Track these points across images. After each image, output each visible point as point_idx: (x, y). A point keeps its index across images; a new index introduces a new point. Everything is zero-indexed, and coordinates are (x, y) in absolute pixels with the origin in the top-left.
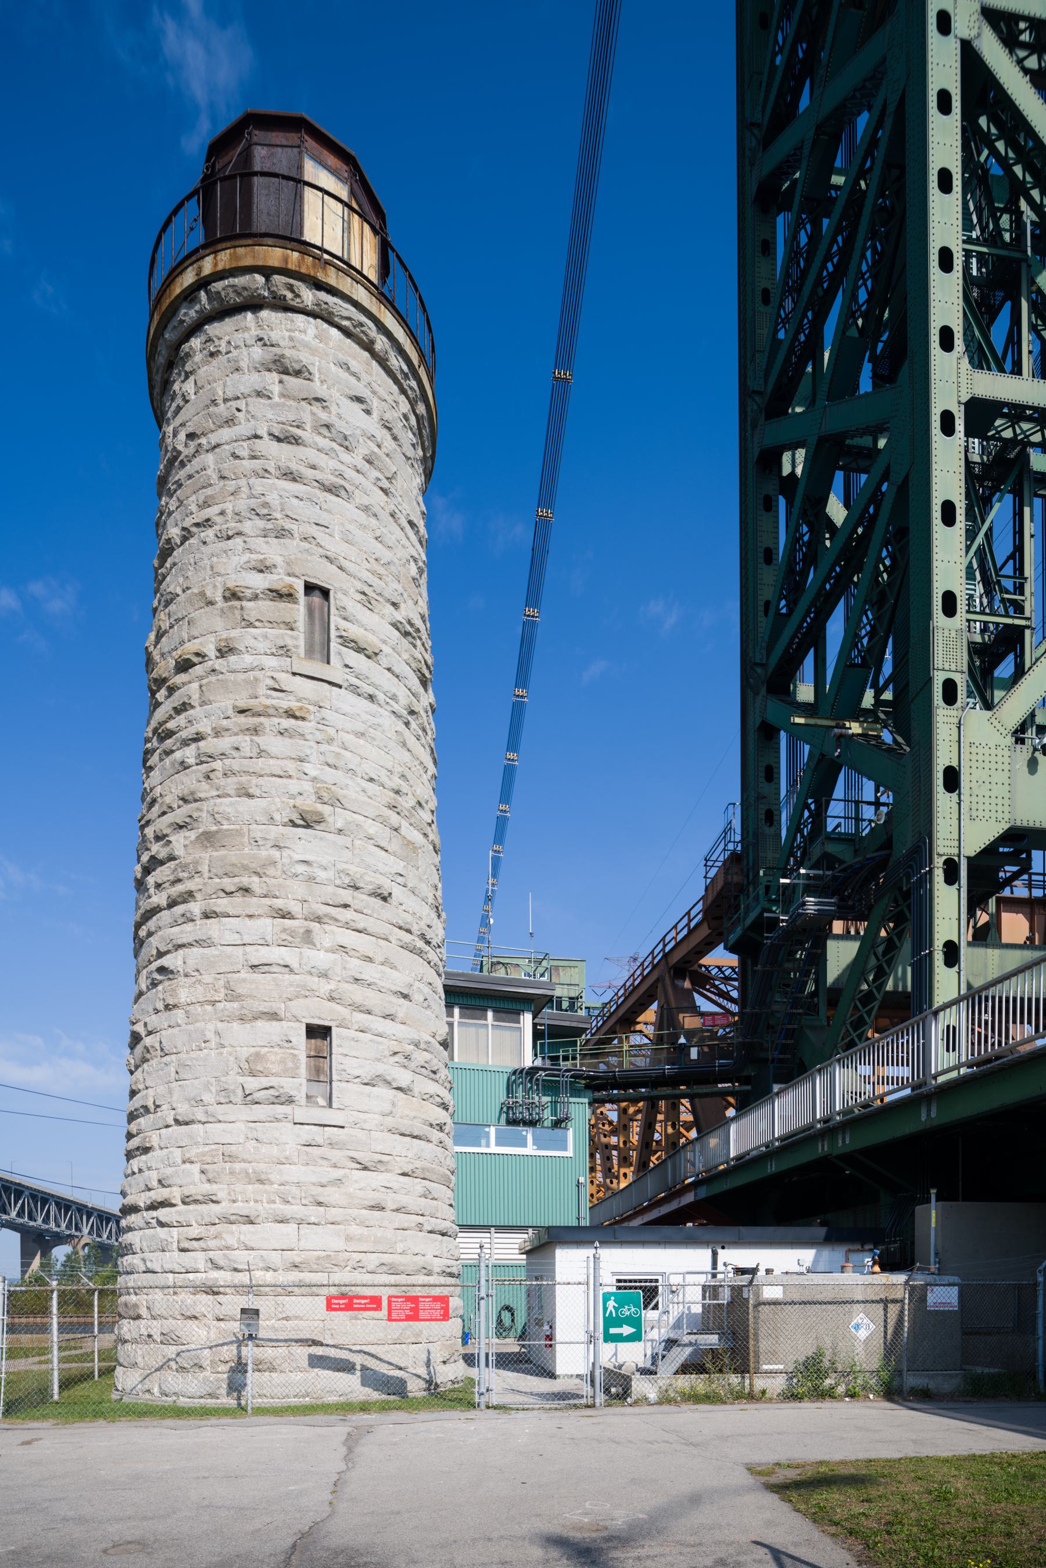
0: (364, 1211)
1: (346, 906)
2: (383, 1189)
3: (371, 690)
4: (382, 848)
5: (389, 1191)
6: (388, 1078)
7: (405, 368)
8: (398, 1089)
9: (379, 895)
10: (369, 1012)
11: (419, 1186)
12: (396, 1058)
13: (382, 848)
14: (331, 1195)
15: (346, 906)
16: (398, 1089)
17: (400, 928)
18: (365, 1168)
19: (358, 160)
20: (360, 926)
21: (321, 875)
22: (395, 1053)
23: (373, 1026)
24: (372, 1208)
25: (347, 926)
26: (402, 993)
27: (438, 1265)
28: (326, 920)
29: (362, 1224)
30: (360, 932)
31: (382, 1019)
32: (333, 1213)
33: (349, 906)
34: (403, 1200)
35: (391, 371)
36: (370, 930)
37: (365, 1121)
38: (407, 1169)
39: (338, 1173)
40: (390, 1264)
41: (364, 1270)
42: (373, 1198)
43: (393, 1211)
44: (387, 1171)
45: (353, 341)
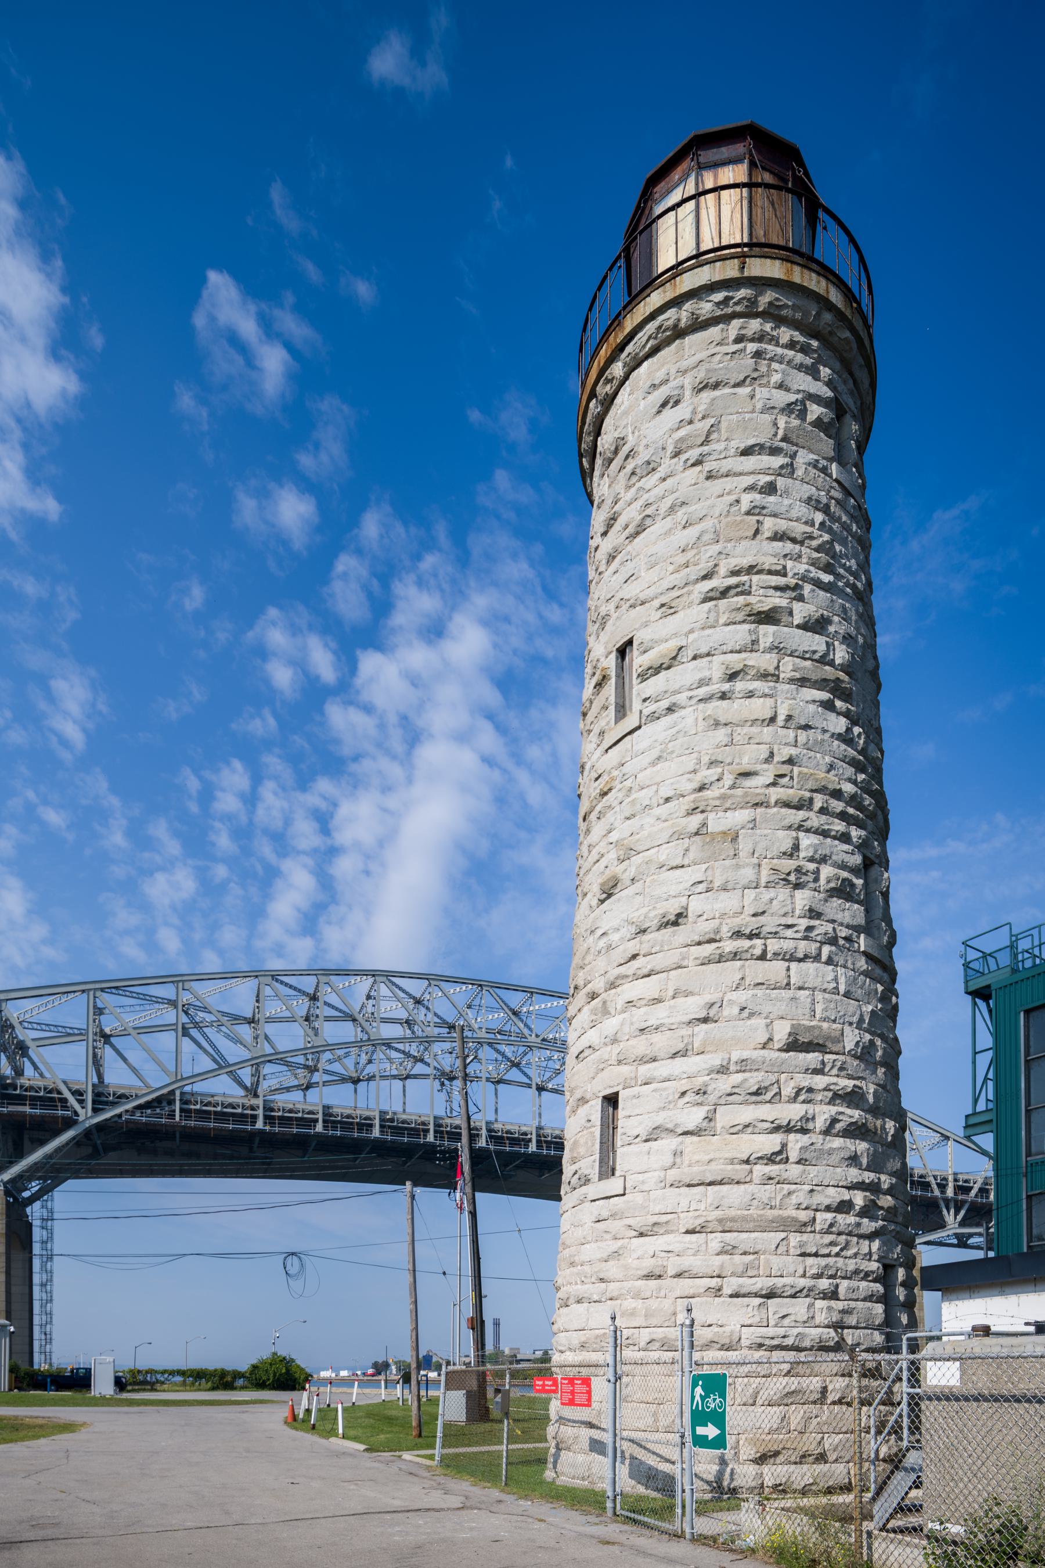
0: (640, 1282)
1: (634, 957)
2: (664, 1254)
3: (665, 704)
4: (677, 867)
5: (670, 1255)
6: (670, 1126)
7: (719, 296)
8: (686, 1133)
9: (667, 923)
10: (654, 1060)
11: (715, 1241)
12: (686, 1099)
13: (677, 867)
14: (612, 1270)
15: (634, 957)
16: (686, 1133)
17: (699, 943)
18: (641, 1235)
19: (701, 132)
20: (645, 971)
21: (615, 937)
22: (684, 1094)
23: (656, 1074)
24: (648, 1276)
25: (637, 977)
26: (698, 1020)
27: (749, 1336)
28: (620, 982)
29: (637, 1295)
30: (649, 975)
31: (670, 1061)
32: (613, 1288)
33: (637, 955)
34: (688, 1262)
35: (713, 318)
36: (658, 968)
37: (643, 1182)
38: (696, 1223)
39: (616, 1245)
40: (661, 1339)
41: (636, 1348)
42: (648, 1265)
43: (674, 1277)
44: (667, 1232)
45: (664, 347)
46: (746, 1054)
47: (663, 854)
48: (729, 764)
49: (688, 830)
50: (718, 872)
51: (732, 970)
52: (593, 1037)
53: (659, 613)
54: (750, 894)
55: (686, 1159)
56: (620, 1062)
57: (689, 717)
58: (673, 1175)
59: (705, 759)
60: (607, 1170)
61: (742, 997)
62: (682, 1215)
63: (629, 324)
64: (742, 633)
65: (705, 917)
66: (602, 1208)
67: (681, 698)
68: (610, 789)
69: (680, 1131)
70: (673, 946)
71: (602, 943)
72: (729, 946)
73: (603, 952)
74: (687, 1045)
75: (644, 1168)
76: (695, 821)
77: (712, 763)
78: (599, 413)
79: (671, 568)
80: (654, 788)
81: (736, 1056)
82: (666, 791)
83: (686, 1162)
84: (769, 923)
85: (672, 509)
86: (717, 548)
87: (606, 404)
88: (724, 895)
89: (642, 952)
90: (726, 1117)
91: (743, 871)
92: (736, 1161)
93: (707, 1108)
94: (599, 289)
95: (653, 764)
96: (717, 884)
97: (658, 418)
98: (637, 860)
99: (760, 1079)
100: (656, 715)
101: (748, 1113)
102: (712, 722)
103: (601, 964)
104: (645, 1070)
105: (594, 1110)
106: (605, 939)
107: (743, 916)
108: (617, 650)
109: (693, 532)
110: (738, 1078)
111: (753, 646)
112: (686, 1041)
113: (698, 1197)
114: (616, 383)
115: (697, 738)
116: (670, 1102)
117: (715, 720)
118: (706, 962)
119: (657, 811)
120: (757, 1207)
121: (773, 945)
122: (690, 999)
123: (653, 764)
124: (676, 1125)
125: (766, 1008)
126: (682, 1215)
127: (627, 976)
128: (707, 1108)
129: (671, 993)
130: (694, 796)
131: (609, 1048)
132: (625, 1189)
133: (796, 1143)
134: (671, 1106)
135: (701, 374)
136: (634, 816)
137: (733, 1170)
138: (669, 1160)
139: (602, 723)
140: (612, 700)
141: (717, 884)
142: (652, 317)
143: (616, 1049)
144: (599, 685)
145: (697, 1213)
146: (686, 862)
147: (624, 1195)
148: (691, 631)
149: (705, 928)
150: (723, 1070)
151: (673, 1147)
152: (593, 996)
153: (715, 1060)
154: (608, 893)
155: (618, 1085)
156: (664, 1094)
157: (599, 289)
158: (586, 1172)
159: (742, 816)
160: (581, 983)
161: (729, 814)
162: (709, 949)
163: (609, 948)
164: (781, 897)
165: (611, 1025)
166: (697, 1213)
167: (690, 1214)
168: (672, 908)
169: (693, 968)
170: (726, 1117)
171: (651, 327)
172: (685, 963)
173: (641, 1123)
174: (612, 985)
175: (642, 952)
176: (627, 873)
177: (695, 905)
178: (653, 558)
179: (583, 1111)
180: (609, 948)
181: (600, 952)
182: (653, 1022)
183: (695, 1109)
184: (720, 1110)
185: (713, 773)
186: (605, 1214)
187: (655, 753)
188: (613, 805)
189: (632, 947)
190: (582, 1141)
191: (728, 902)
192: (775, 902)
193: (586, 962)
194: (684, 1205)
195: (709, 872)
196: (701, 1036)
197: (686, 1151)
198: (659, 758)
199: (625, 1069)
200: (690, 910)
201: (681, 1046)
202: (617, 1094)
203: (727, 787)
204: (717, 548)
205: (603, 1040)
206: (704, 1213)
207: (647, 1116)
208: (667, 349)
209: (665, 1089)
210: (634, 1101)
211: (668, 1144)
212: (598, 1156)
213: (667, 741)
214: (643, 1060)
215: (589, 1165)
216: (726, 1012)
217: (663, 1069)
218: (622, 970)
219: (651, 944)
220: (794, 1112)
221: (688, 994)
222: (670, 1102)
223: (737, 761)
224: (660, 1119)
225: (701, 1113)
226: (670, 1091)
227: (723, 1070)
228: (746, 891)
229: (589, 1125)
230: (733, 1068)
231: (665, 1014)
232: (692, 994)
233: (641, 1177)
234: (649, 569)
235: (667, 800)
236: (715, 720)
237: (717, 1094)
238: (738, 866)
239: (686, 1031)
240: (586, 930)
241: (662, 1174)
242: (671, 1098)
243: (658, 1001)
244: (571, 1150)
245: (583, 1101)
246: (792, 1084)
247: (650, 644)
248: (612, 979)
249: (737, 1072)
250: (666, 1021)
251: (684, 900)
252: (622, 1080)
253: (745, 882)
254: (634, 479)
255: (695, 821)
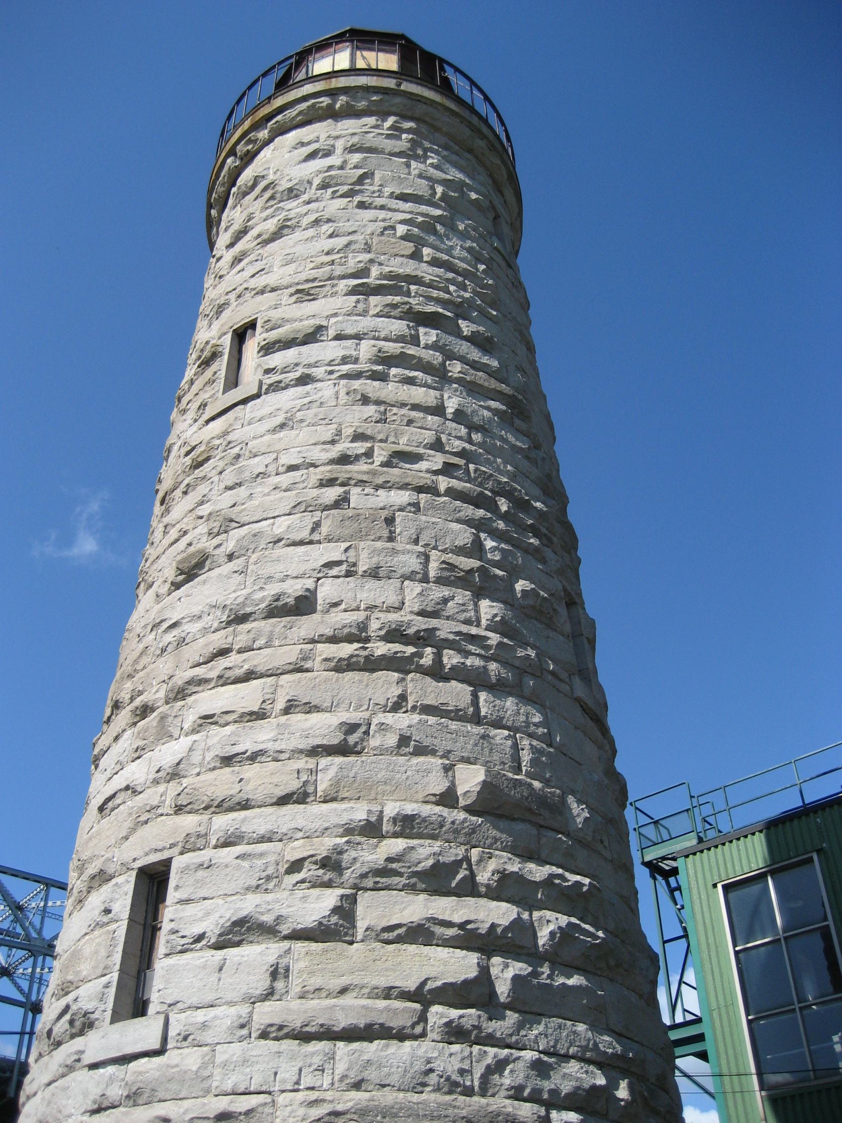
6: (268, 918)
13: (301, 543)
20: (239, 672)
21: (193, 628)
25: (223, 681)
36: (261, 669)
37: (204, 1026)
46: (410, 808)
47: (280, 527)
48: (381, 441)
49: (320, 501)
50: (364, 555)
51: (386, 685)
52: (137, 772)
53: (294, 298)
54: (413, 589)
55: (295, 984)
56: (179, 809)
57: (325, 390)
58: (266, 1013)
59: (348, 431)
60: (133, 1002)
61: (403, 721)
62: (282, 1099)
63: (279, 102)
64: (399, 326)
65: (343, 606)
66: (112, 1082)
67: (319, 372)
68: (208, 459)
69: (285, 929)
70: (288, 641)
71: (169, 637)
72: (381, 649)
73: (169, 649)
74: (305, 783)
75: (209, 998)
76: (332, 494)
77: (358, 437)
78: (236, 167)
79: (312, 265)
80: (274, 456)
81: (391, 809)
82: (288, 459)
83: (296, 989)
84: (445, 629)
85: (317, 222)
86: (368, 256)
87: (245, 160)
88: (371, 584)
89: (236, 647)
90: (372, 911)
91: (402, 558)
92: (395, 993)
93: (341, 891)
94: (250, 88)
95: (274, 431)
96: (361, 568)
97: (304, 165)
98: (236, 534)
99: (436, 849)
100: (282, 385)
101: (416, 908)
102: (359, 397)
103: (164, 666)
104: (223, 823)
105: (121, 895)
106: (175, 632)
107: (402, 613)
108: (234, 331)
109: (340, 242)
110: (398, 845)
111: (415, 340)
112: (304, 778)
113: (317, 1061)
114: (259, 144)
115: (338, 410)
116: (268, 878)
117: (362, 395)
118: (343, 666)
119: (275, 480)
120: (438, 1089)
121: (451, 659)
122: (315, 718)
123: (274, 431)
124: (279, 919)
125: (443, 745)
126: (282, 1099)
127: (207, 681)
128: (341, 891)
129: (281, 704)
130: (329, 468)
131: (161, 788)
132: (165, 1039)
133: (505, 973)
134: (271, 886)
135: (355, 139)
136: (240, 485)
137: (387, 1009)
138: (261, 984)
139: (204, 396)
140: (222, 374)
141: (361, 568)
142: (305, 98)
143: (173, 789)
144: (206, 363)
145: (313, 1095)
146: (316, 537)
147: (160, 1052)
148: (335, 315)
149: (340, 619)
150: (372, 829)
151: (272, 959)
152: (145, 711)
153: (359, 813)
154: (191, 571)
155: (172, 846)
156: (259, 863)
157: (250, 88)
158: (88, 1006)
159: (403, 497)
160: (125, 696)
161: (381, 492)
162: (347, 650)
163: (181, 642)
164: (459, 599)
165: (167, 754)
166: (313, 1095)
167: (300, 1096)
168: (294, 589)
169: (321, 675)
170: (372, 911)
171: (304, 106)
172: (308, 665)
173: (208, 914)
174: (180, 694)
175: (236, 647)
176: (222, 549)
177: (327, 591)
178: (290, 257)
179: (96, 900)
180: (181, 642)
181: (163, 650)
182: (247, 745)
183: (316, 892)
184: (364, 900)
185: (360, 447)
186: (116, 1092)
187: (280, 419)
188: (209, 475)
189: (218, 640)
190: (87, 950)
191: (383, 592)
192: (450, 604)
193: (139, 667)
194: (288, 1074)
195: (352, 553)
196: (332, 773)
197: (295, 968)
198: (282, 426)
199: (189, 822)
200: (320, 596)
201: (294, 785)
202: (167, 863)
203: (377, 463)
204: (368, 256)
205: (152, 776)
206: (328, 1095)
207: (220, 901)
208: (318, 124)
209: (262, 855)
210: (201, 873)
211: (258, 954)
212: (116, 975)
213: (295, 410)
214: (222, 806)
215: (96, 992)
216: (374, 742)
217: (257, 821)
218: (200, 672)
219: (251, 635)
220: (499, 914)
221: (311, 708)
222: (268, 878)
223: (391, 439)
224: (248, 905)
225: (330, 898)
226: (272, 858)
227: (372, 829)
228: (406, 583)
229: (105, 919)
230: (386, 827)
231: (272, 735)
232: (317, 709)
233: (200, 1016)
234: (283, 265)
235: (292, 468)
236: (362, 395)
237: (359, 868)
238: (395, 552)
239: (303, 763)
240: (145, 626)
241: (244, 1010)
242: (270, 870)
243: (259, 715)
244: (65, 969)
245: (102, 877)
246: (492, 865)
247: (279, 322)
248: (180, 683)
249: (396, 835)
250: (270, 746)
251: (309, 583)
252: (180, 837)
253: (407, 570)
254: (272, 203)
255: (332, 494)
